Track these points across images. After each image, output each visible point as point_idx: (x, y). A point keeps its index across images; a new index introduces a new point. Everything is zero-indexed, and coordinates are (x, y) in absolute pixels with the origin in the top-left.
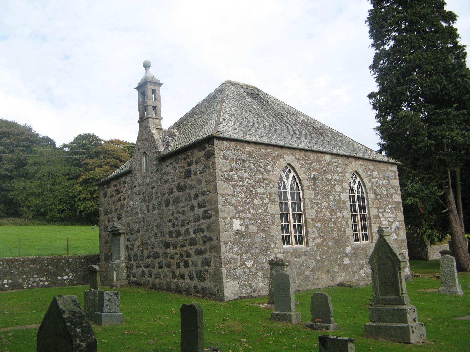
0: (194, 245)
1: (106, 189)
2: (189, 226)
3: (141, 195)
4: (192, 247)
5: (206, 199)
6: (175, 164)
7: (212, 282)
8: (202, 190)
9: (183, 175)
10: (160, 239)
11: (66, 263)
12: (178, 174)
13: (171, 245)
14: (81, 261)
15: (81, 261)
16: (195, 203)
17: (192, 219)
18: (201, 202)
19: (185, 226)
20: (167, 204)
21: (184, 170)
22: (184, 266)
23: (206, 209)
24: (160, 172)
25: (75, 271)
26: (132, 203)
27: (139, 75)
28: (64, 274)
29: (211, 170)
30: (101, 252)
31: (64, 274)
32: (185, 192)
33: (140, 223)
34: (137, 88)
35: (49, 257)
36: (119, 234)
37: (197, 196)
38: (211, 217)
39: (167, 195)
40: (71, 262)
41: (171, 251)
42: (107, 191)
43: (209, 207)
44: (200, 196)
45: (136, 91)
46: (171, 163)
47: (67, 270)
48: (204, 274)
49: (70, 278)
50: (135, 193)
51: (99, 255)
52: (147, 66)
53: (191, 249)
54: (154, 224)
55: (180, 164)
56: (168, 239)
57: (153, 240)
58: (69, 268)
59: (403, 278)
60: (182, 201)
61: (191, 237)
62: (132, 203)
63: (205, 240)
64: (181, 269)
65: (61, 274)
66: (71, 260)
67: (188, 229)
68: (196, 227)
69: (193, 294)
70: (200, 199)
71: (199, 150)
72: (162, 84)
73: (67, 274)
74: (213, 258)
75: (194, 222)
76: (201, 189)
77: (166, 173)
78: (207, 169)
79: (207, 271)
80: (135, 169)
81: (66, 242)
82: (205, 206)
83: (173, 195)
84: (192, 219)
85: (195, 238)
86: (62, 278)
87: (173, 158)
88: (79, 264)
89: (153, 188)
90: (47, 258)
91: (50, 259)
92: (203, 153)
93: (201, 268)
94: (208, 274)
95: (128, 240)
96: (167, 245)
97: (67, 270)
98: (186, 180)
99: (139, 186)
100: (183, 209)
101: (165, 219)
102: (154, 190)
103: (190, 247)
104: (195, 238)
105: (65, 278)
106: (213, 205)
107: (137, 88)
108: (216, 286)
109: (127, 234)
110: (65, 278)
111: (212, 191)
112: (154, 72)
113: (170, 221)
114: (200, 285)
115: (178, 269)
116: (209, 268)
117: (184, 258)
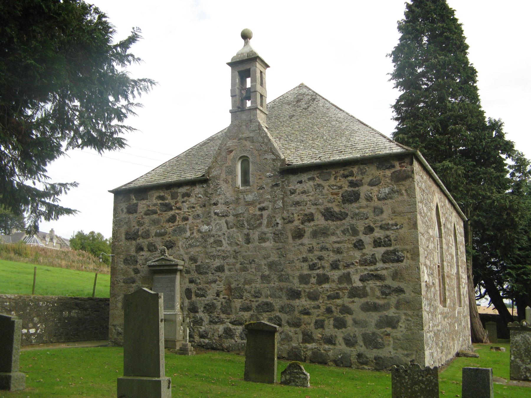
0: (361, 298)
1: (135, 201)
2: (351, 270)
3: (231, 217)
4: (356, 299)
5: (392, 235)
6: (318, 181)
7: (400, 350)
8: (384, 222)
9: (339, 198)
10: (275, 284)
11: (35, 308)
12: (327, 194)
13: (303, 294)
14: (54, 306)
15: (54, 306)
16: (367, 239)
17: (358, 261)
18: (380, 238)
19: (339, 269)
20: (299, 234)
21: (341, 192)
22: (334, 325)
23: (391, 248)
24: (283, 187)
25: (44, 321)
26: (205, 228)
27: (236, 47)
28: (30, 325)
29: (405, 197)
30: (113, 294)
31: (30, 325)
32: (343, 221)
33: (224, 258)
34: (233, 64)
35: (13, 297)
36: (175, 271)
37: (370, 230)
38: (402, 261)
39: (296, 223)
40: (41, 307)
41: (303, 302)
42: (136, 205)
43: (396, 247)
44: (377, 230)
45: (229, 68)
46: (313, 179)
47: (35, 319)
48: (382, 338)
49: (38, 331)
50: (216, 214)
51: (107, 300)
52: (246, 36)
53: (353, 302)
54: (263, 262)
55: (332, 181)
56: (296, 284)
57: (258, 286)
58: (37, 316)
59: (385, 329)
60: (333, 234)
61: (354, 285)
62: (205, 228)
63: (387, 291)
64: (327, 330)
65: (27, 324)
66: (41, 303)
67: (349, 274)
68: (366, 272)
69: (354, 366)
70: (378, 234)
71: (378, 168)
72: (229, 64)
73: (35, 326)
74: (403, 317)
75: (361, 265)
76: (381, 221)
77: (297, 191)
78: (396, 195)
79: (388, 335)
80: (217, 178)
81: (32, 277)
82: (390, 245)
83: (312, 224)
84: (358, 261)
85: (364, 287)
86: (28, 331)
87: (318, 172)
88: (51, 310)
89: (262, 209)
90: (10, 299)
91: (13, 299)
92: (388, 173)
93: (375, 330)
94: (391, 339)
95: (191, 281)
96: (295, 294)
97: (35, 319)
98: (346, 205)
99: (226, 203)
100: (337, 245)
101: (290, 256)
102: (265, 213)
103: (351, 300)
104: (364, 287)
105: (32, 331)
106: (407, 245)
107: (233, 64)
108: (407, 355)
109: (188, 272)
110: (32, 331)
111: (405, 225)
112: (256, 46)
113: (305, 260)
114: (371, 354)
115: (320, 330)
116: (395, 330)
117: (335, 314)
